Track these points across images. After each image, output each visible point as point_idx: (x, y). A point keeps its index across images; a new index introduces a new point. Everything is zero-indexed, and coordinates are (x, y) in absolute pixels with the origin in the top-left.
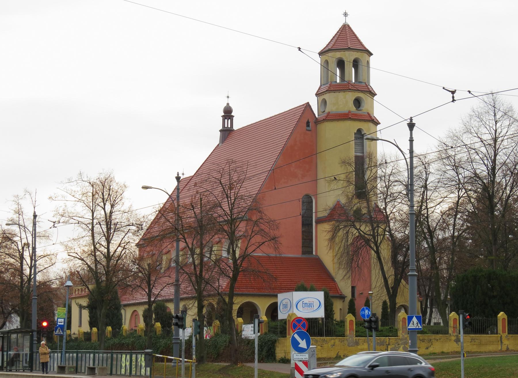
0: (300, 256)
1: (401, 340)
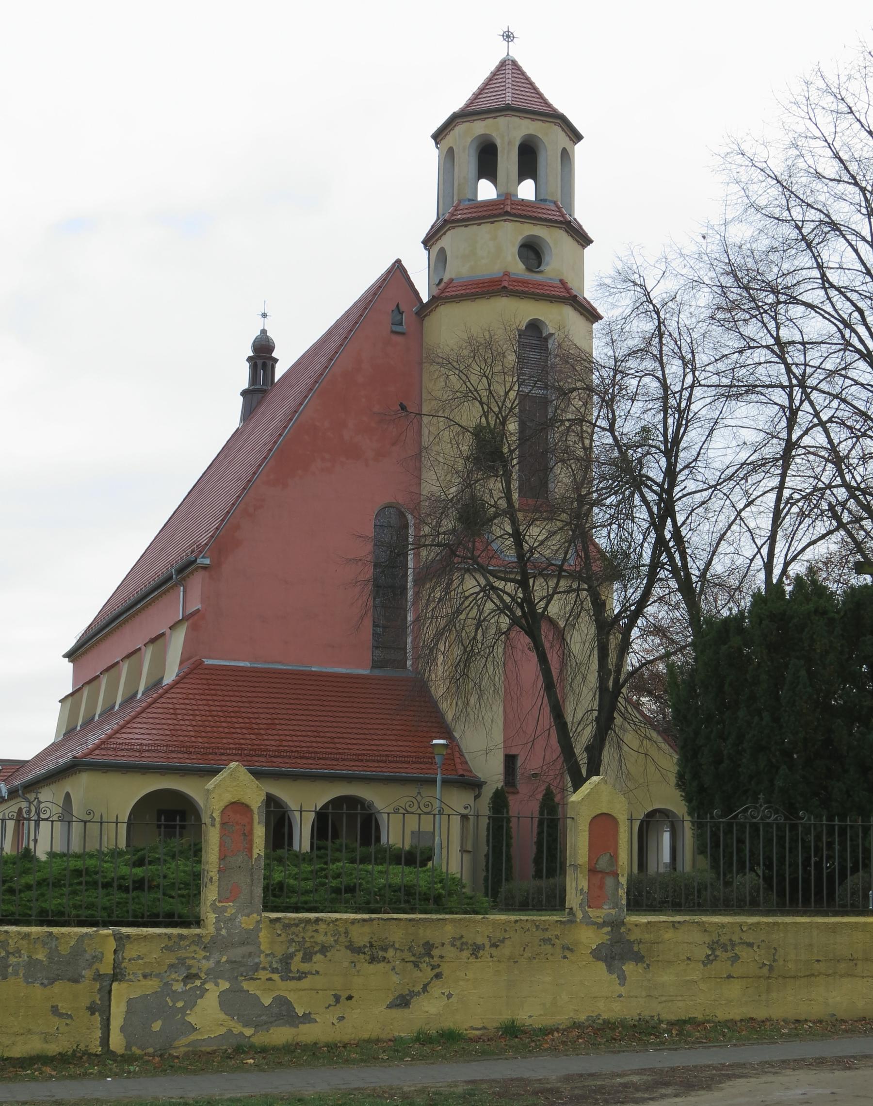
0: (366, 672)
1: (209, 946)
